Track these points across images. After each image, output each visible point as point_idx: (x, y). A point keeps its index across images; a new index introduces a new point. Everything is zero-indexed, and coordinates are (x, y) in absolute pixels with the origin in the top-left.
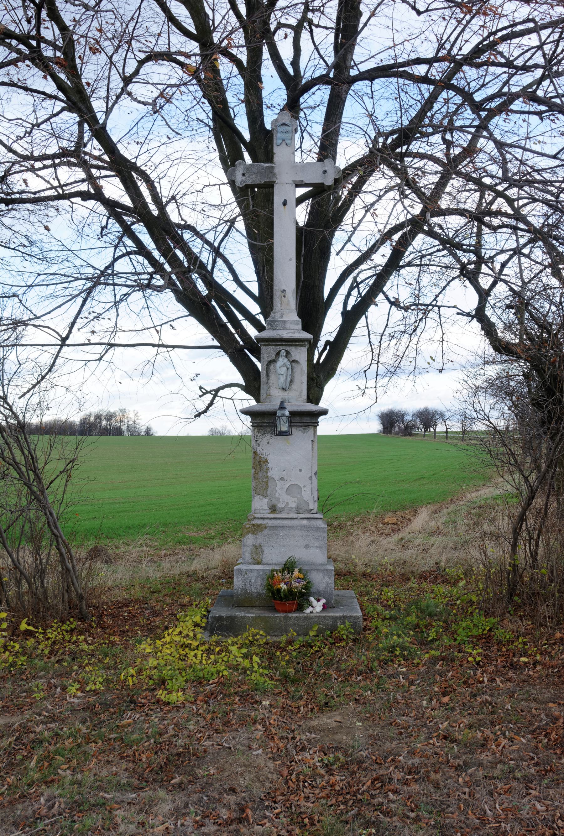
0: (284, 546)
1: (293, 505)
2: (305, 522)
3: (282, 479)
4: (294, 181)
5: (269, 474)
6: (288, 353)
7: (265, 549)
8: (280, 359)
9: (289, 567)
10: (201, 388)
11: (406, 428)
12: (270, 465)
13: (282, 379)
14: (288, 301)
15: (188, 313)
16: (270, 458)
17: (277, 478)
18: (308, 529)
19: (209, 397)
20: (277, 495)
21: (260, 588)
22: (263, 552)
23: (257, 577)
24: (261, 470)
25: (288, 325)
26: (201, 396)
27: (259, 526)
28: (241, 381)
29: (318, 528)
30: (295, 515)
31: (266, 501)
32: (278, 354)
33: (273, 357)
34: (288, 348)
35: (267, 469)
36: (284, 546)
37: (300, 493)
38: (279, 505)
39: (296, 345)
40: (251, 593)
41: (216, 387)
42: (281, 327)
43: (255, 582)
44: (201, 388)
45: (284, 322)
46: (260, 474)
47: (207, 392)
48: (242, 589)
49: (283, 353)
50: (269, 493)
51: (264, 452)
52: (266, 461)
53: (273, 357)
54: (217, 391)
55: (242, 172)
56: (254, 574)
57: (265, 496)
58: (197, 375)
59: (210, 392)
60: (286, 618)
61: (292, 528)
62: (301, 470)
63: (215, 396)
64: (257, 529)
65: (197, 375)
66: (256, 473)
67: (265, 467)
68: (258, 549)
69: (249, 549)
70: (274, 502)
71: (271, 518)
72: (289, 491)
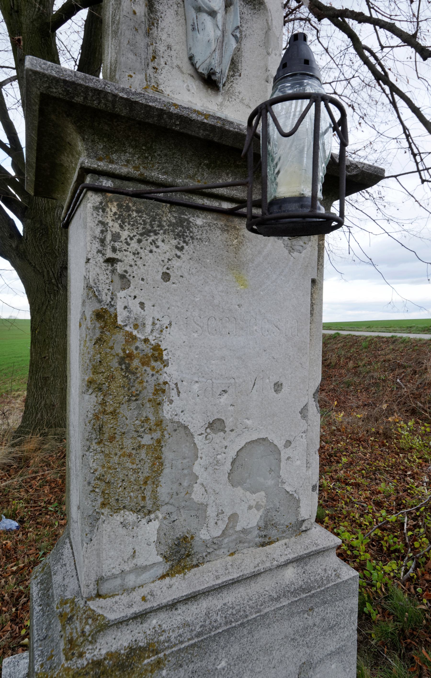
1: (250, 519)
5: (167, 411)
12: (171, 373)
15: (14, 66)
16: (172, 342)
20: (197, 495)
24: (133, 397)
31: (150, 529)
35: (160, 389)
37: (275, 470)
38: (204, 535)
46: (129, 415)
50: (163, 491)
51: (149, 314)
52: (157, 354)
57: (144, 511)
62: (278, 387)
67: (150, 383)
70: (184, 523)
72: (238, 472)
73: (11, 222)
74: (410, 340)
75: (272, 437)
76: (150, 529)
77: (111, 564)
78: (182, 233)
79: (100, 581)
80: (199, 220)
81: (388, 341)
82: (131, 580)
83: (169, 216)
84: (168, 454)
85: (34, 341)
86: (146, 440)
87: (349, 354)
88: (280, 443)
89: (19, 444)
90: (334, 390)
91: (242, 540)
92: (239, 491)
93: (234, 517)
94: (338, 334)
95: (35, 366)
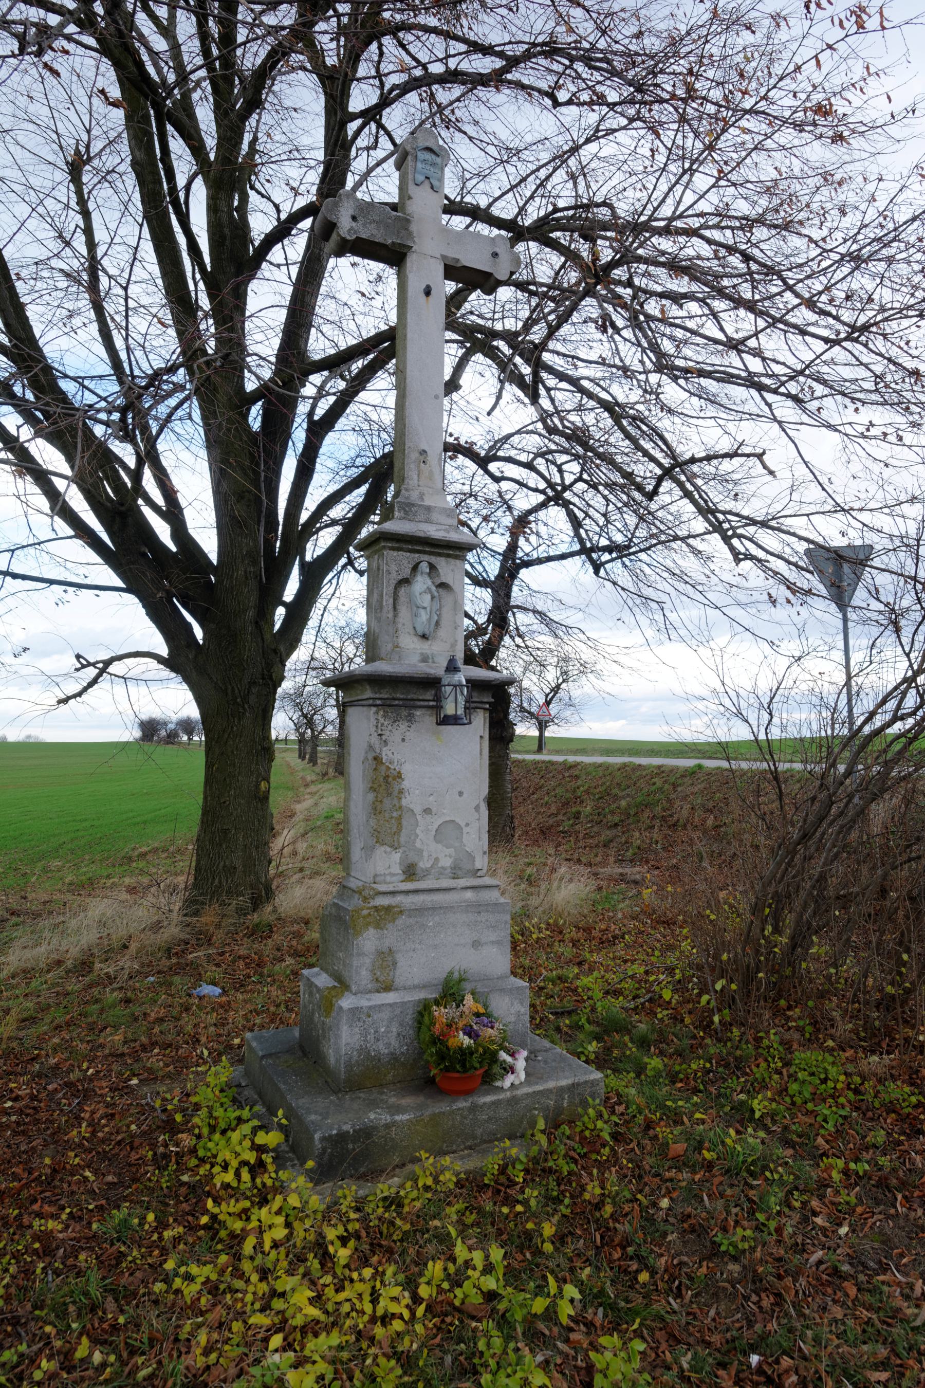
0: (435, 947)
1: (446, 862)
2: (469, 895)
3: (427, 811)
4: (444, 257)
5: (404, 802)
6: (432, 567)
7: (399, 957)
8: (419, 578)
9: (450, 991)
10: (78, 657)
11: (169, 736)
12: (406, 784)
13: (424, 616)
14: (431, 472)
16: (406, 770)
17: (418, 809)
18: (478, 907)
19: (92, 672)
21: (394, 1043)
22: (395, 964)
23: (391, 1020)
24: (390, 795)
25: (435, 516)
26: (77, 670)
27: (388, 909)
28: (164, 651)
29: (495, 907)
30: (445, 883)
31: (397, 857)
32: (415, 568)
33: (406, 572)
34: (433, 559)
35: (401, 792)
36: (435, 947)
38: (422, 865)
39: (448, 556)
40: (378, 1058)
41: (106, 656)
42: (422, 517)
43: (387, 1032)
44: (78, 657)
45: (429, 509)
46: (387, 801)
47: (89, 664)
48: (361, 1050)
49: (424, 567)
51: (396, 757)
52: (399, 776)
53: (406, 572)
54: (107, 663)
55: (351, 212)
56: (385, 1015)
57: (395, 848)
58: (25, 650)
59: (93, 665)
60: (474, 1108)
61: (448, 908)
62: (461, 794)
63: (102, 671)
64: (387, 914)
65: (25, 650)
66: (377, 802)
68: (386, 959)
69: (368, 961)
70: (413, 857)
71: (407, 892)
72: (439, 835)
73: (189, 626)
74: (673, 770)
75: (458, 820)
76: (397, 857)
77: (381, 870)
78: (410, 719)
79: (375, 876)
80: (418, 713)
81: (692, 773)
82: (388, 879)
83: (405, 713)
84: (404, 823)
85: (208, 781)
86: (395, 814)
87: (710, 805)
88: (463, 824)
89: (196, 913)
90: (675, 867)
91: (441, 873)
92: (440, 846)
93: (437, 859)
94: (700, 767)
95: (211, 814)
